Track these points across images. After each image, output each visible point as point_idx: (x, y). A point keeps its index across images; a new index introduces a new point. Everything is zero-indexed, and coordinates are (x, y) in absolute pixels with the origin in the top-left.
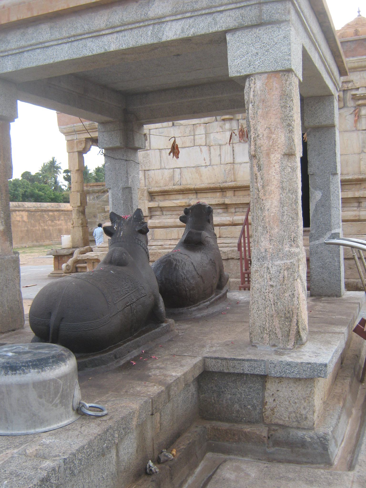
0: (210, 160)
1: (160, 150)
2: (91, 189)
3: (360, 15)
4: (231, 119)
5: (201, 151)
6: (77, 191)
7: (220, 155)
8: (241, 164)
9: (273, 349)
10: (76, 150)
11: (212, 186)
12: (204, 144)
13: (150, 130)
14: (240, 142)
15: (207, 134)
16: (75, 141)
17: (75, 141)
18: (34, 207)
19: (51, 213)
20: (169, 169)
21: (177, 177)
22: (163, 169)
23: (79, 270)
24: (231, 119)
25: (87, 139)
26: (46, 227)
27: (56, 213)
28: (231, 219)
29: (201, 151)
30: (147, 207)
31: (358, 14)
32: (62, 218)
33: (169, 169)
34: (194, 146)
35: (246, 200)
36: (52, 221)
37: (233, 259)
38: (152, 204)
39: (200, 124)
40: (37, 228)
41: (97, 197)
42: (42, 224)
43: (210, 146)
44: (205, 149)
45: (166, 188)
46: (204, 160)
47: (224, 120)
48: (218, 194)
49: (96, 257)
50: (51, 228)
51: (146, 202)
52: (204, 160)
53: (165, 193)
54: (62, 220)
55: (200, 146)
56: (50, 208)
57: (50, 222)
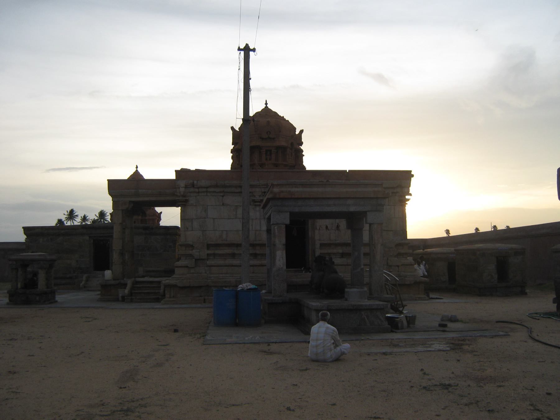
1: (214, 219)
3: (266, 107)
25: (130, 201)
38: (209, 252)
53: (217, 246)
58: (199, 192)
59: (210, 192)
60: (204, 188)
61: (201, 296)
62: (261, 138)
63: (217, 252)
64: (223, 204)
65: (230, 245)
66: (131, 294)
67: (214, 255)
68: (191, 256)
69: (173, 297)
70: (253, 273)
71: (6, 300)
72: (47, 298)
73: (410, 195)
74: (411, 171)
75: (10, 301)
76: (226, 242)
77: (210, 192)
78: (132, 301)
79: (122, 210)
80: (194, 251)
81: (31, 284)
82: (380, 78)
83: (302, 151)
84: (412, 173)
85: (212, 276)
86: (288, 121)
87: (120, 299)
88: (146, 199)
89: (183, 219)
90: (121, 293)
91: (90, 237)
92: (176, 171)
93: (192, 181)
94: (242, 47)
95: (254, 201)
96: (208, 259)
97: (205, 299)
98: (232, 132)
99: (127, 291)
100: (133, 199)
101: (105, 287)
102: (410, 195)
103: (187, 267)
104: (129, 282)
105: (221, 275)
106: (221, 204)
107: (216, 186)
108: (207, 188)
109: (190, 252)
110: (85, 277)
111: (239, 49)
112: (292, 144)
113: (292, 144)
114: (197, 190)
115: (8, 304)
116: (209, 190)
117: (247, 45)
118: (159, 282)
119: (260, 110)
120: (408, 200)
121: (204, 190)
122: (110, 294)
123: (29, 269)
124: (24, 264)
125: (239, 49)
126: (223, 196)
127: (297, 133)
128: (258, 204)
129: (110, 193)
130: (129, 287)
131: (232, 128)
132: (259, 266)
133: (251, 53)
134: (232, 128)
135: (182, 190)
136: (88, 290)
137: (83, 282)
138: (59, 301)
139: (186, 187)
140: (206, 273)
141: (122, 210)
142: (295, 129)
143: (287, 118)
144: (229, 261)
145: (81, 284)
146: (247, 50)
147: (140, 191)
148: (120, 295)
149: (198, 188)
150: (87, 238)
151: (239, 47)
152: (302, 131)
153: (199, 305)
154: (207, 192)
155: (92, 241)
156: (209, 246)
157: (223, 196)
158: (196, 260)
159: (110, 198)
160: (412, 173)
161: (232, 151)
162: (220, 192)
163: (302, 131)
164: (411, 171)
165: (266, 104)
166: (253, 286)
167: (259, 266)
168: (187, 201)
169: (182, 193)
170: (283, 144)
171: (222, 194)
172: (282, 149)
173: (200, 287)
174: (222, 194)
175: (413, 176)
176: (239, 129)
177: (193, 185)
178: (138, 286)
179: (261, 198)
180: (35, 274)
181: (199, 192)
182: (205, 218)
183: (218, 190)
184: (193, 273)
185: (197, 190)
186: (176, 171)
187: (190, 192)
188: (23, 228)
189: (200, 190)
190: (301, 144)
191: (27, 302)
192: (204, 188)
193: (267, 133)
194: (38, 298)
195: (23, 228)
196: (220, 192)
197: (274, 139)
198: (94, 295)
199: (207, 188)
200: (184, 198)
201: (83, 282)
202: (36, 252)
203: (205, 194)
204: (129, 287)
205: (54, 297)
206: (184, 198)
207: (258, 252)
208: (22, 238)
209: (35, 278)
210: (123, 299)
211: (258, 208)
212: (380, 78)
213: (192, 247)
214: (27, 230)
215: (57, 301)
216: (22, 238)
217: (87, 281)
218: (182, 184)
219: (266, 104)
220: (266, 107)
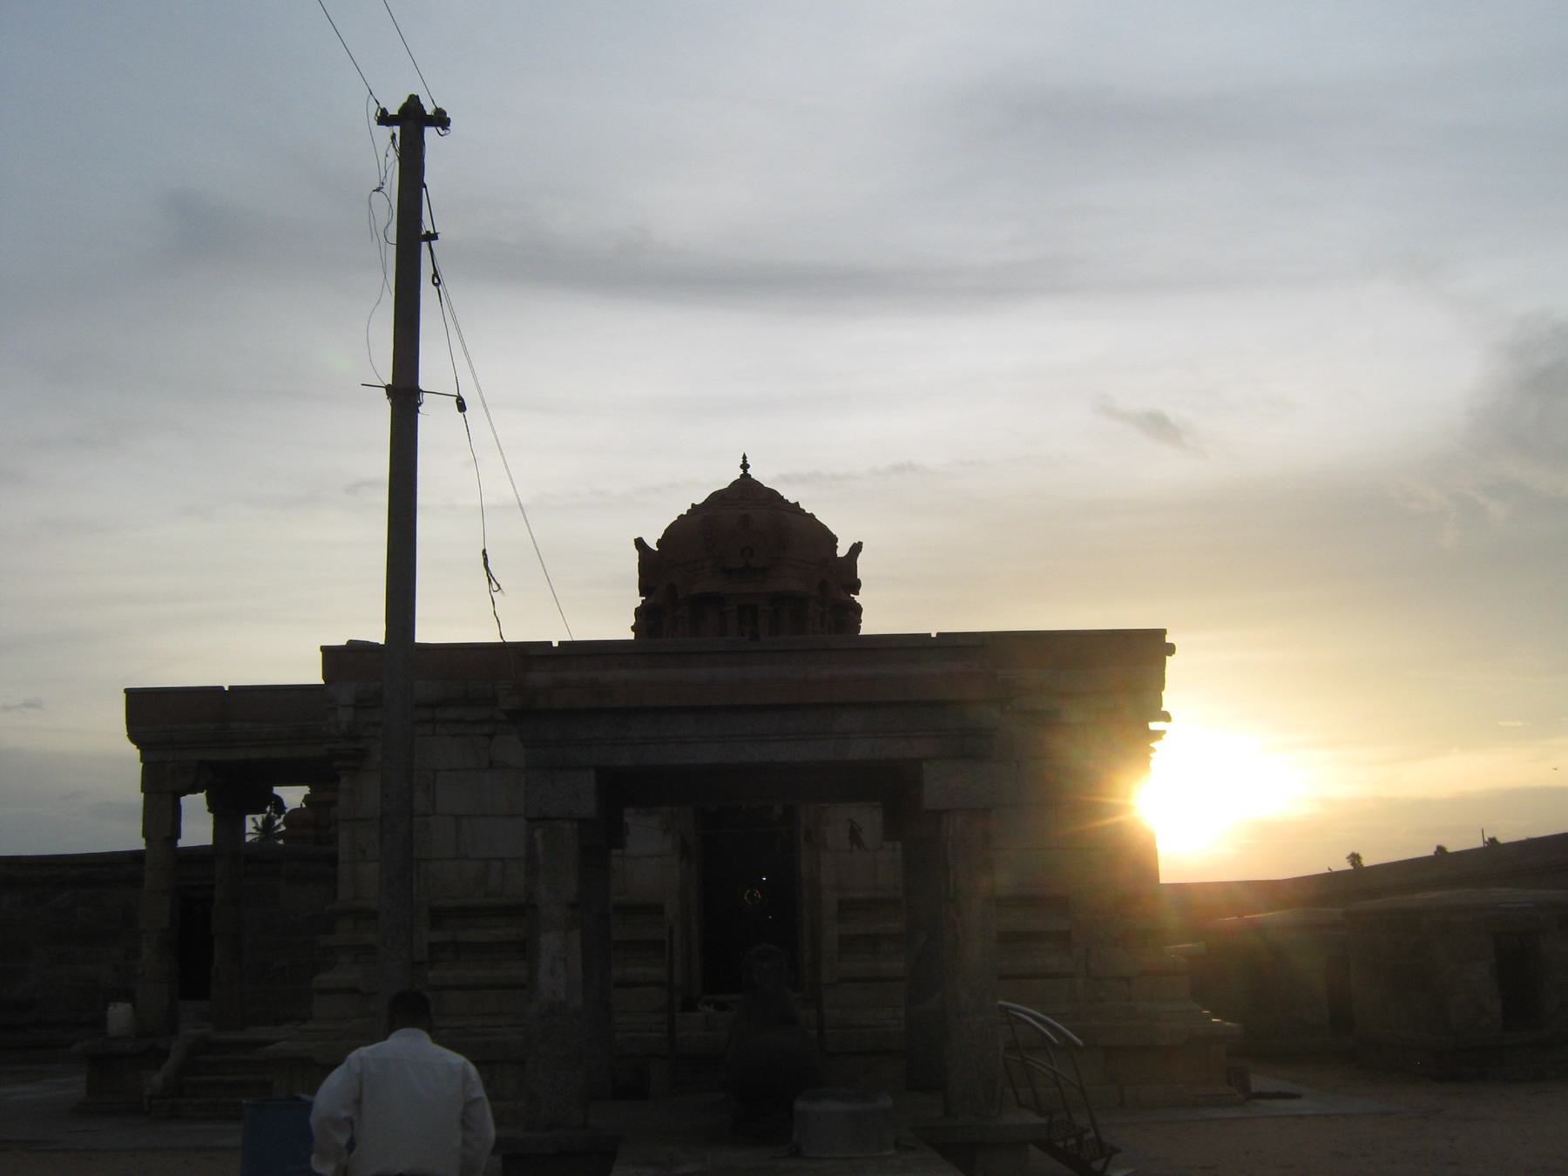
3: (745, 476)
73: (1166, 717)
74: (1163, 632)
82: (1158, 425)
83: (858, 609)
84: (1168, 640)
86: (812, 516)
89: (193, 790)
92: (326, 651)
94: (393, 110)
102: (1166, 717)
111: (384, 119)
117: (414, 100)
120: (1158, 735)
125: (384, 119)
126: (491, 736)
129: (134, 736)
131: (640, 543)
133: (430, 133)
134: (640, 543)
142: (833, 539)
146: (413, 123)
151: (384, 111)
152: (856, 548)
159: (134, 752)
160: (1168, 640)
161: (638, 612)
163: (856, 548)
164: (1163, 632)
165: (745, 466)
166: (1080, 1042)
175: (1171, 649)
176: (659, 543)
186: (326, 651)
190: (856, 586)
198: (71, 1086)
212: (1158, 425)
219: (745, 466)
220: (745, 476)
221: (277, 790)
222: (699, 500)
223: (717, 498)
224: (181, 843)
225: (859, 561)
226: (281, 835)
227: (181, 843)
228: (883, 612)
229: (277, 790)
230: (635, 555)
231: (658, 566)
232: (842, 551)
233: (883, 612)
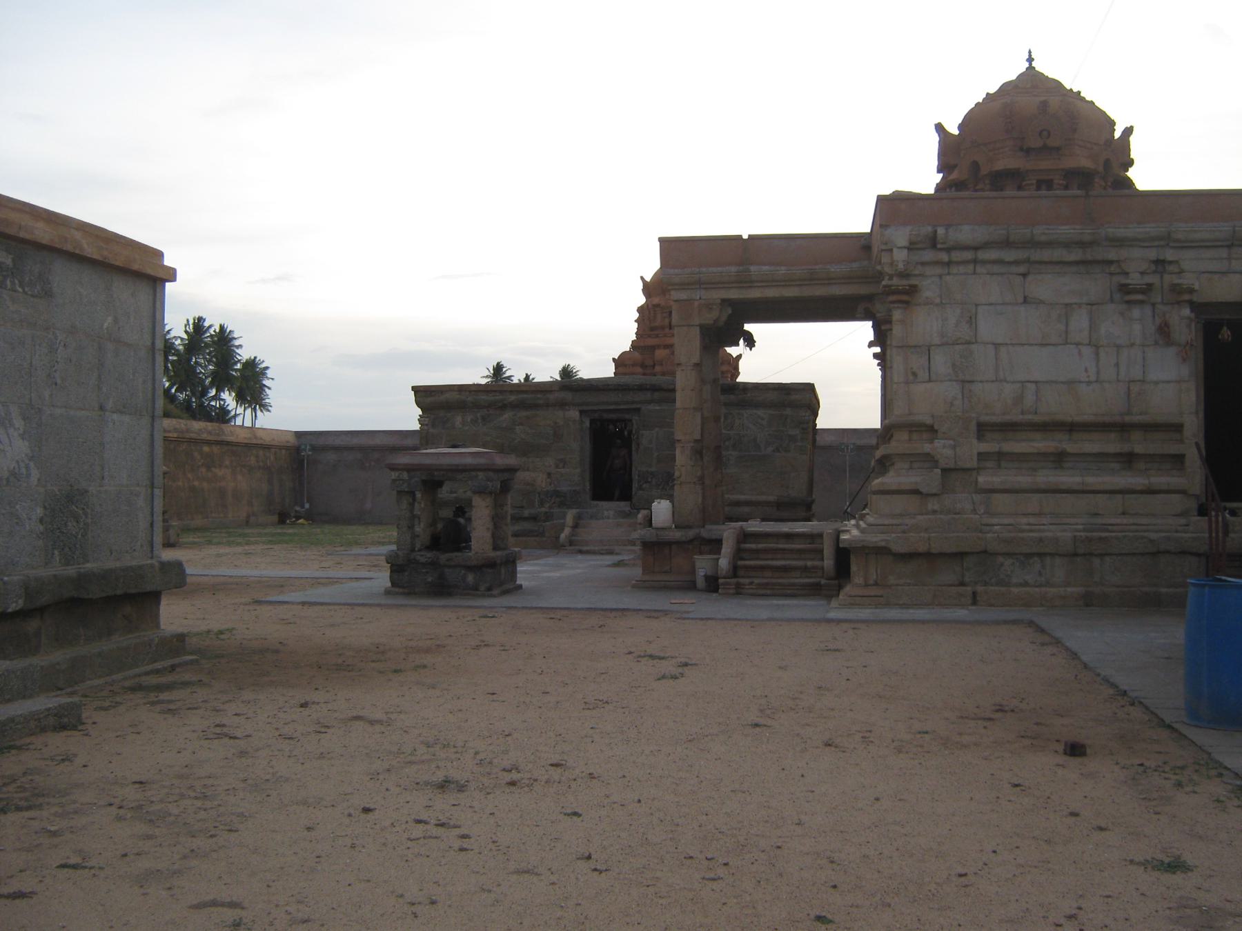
0: (1098, 373)
1: (996, 346)
2: (470, 399)
3: (1031, 68)
4: (1142, 302)
5: (1080, 354)
6: (694, 408)
7: (1117, 365)
8: (1156, 383)
9: (463, 831)
10: (697, 321)
11: (1107, 419)
12: (1087, 341)
13: (977, 305)
14: (1156, 343)
15: (1093, 327)
16: (696, 303)
17: (696, 303)
18: (176, 430)
19: (206, 449)
20: (1013, 382)
21: (1030, 399)
22: (1001, 381)
23: (741, 573)
24: (1142, 302)
25: (724, 301)
26: (196, 483)
27: (216, 449)
28: (1146, 482)
29: (1080, 354)
30: (975, 452)
31: (1027, 65)
32: (227, 463)
33: (1013, 382)
34: (1066, 343)
35: (1173, 449)
36: (209, 468)
37: (1168, 552)
38: (984, 447)
39: (1080, 305)
40: (180, 483)
41: (483, 418)
42: (189, 475)
43: (1097, 347)
44: (1087, 351)
45: (1007, 418)
46: (1086, 370)
47: (1128, 302)
48: (1113, 435)
49: (883, 544)
50: (205, 485)
51: (975, 441)
52: (1086, 370)
53: (1009, 428)
54: (226, 467)
55: (1077, 344)
56: (205, 436)
57: (204, 470)
58: (949, 264)
59: (984, 262)
60: (966, 248)
61: (962, 584)
62: (1021, 149)
63: (1070, 447)
64: (1026, 300)
65: (1047, 427)
66: (735, 570)
67: (1000, 456)
68: (930, 460)
69: (876, 584)
70: (1124, 513)
71: (383, 578)
72: (496, 576)
75: (393, 584)
76: (1036, 419)
77: (984, 262)
78: (739, 591)
79: (701, 327)
80: (938, 443)
81: (451, 536)
85: (995, 521)
86: (1092, 103)
87: (700, 582)
88: (771, 293)
90: (703, 565)
91: (581, 412)
93: (930, 229)
95: (1125, 289)
96: (978, 470)
97: (974, 594)
98: (937, 139)
99: (724, 563)
100: (734, 294)
101: (656, 549)
103: (916, 492)
104: (728, 533)
105: (1025, 520)
106: (1021, 300)
107: (1007, 244)
108: (976, 249)
109: (927, 448)
110: (570, 515)
112: (1107, 163)
113: (1107, 163)
114: (944, 257)
115: (387, 593)
116: (982, 255)
118: (815, 537)
119: (1013, 77)
121: (968, 255)
122: (669, 565)
123: (444, 493)
124: (432, 481)
126: (1024, 275)
127: (1117, 135)
128: (1140, 297)
130: (727, 549)
131: (939, 128)
132: (1142, 492)
134: (939, 128)
135: (900, 256)
136: (581, 552)
137: (567, 531)
138: (525, 584)
139: (912, 247)
140: (974, 511)
141: (701, 327)
142: (1113, 123)
143: (1088, 95)
144: (1046, 477)
145: (563, 536)
147: (752, 268)
148: (701, 573)
149: (949, 250)
150: (574, 414)
152: (1128, 131)
153: (961, 613)
154: (975, 261)
155: (587, 424)
156: (983, 429)
157: (1024, 275)
158: (944, 471)
162: (1016, 263)
163: (1128, 131)
165: (1030, 60)
167: (1142, 492)
168: (913, 290)
169: (901, 266)
170: (1085, 163)
171: (1022, 269)
172: (1081, 178)
173: (961, 555)
174: (1022, 269)
176: (960, 127)
177: (933, 242)
178: (753, 546)
179: (1148, 279)
180: (462, 510)
181: (949, 264)
182: (969, 343)
183: (1010, 255)
184: (934, 512)
185: (944, 257)
187: (923, 264)
188: (413, 388)
189: (957, 256)
191: (441, 589)
192: (966, 248)
193: (1040, 134)
194: (470, 578)
195: (413, 388)
196: (1016, 263)
197: (1058, 149)
199: (976, 249)
200: (905, 282)
201: (567, 531)
202: (464, 446)
203: (971, 267)
204: (727, 549)
205: (513, 573)
206: (905, 282)
207: (1139, 449)
208: (408, 418)
209: (461, 520)
210: (713, 585)
211: (1136, 312)
213: (930, 430)
214: (423, 395)
215: (520, 587)
216: (408, 418)
217: (575, 526)
218: (900, 236)
219: (1030, 60)
220: (1031, 68)
221: (747, 327)
222: (993, 90)
223: (1006, 88)
224: (739, 380)
225: (1131, 138)
226: (236, 370)
227: (739, 380)
228: (1150, 173)
229: (747, 327)
230: (935, 139)
231: (952, 151)
232: (167, 328)
233: (1150, 173)
